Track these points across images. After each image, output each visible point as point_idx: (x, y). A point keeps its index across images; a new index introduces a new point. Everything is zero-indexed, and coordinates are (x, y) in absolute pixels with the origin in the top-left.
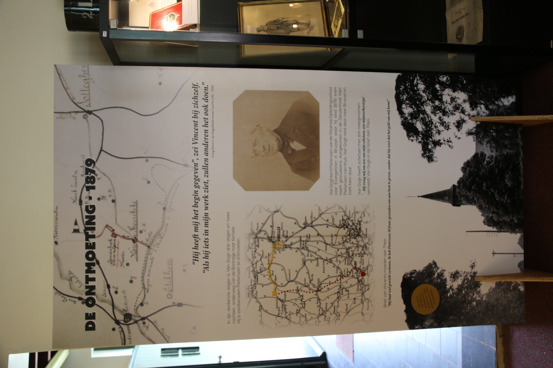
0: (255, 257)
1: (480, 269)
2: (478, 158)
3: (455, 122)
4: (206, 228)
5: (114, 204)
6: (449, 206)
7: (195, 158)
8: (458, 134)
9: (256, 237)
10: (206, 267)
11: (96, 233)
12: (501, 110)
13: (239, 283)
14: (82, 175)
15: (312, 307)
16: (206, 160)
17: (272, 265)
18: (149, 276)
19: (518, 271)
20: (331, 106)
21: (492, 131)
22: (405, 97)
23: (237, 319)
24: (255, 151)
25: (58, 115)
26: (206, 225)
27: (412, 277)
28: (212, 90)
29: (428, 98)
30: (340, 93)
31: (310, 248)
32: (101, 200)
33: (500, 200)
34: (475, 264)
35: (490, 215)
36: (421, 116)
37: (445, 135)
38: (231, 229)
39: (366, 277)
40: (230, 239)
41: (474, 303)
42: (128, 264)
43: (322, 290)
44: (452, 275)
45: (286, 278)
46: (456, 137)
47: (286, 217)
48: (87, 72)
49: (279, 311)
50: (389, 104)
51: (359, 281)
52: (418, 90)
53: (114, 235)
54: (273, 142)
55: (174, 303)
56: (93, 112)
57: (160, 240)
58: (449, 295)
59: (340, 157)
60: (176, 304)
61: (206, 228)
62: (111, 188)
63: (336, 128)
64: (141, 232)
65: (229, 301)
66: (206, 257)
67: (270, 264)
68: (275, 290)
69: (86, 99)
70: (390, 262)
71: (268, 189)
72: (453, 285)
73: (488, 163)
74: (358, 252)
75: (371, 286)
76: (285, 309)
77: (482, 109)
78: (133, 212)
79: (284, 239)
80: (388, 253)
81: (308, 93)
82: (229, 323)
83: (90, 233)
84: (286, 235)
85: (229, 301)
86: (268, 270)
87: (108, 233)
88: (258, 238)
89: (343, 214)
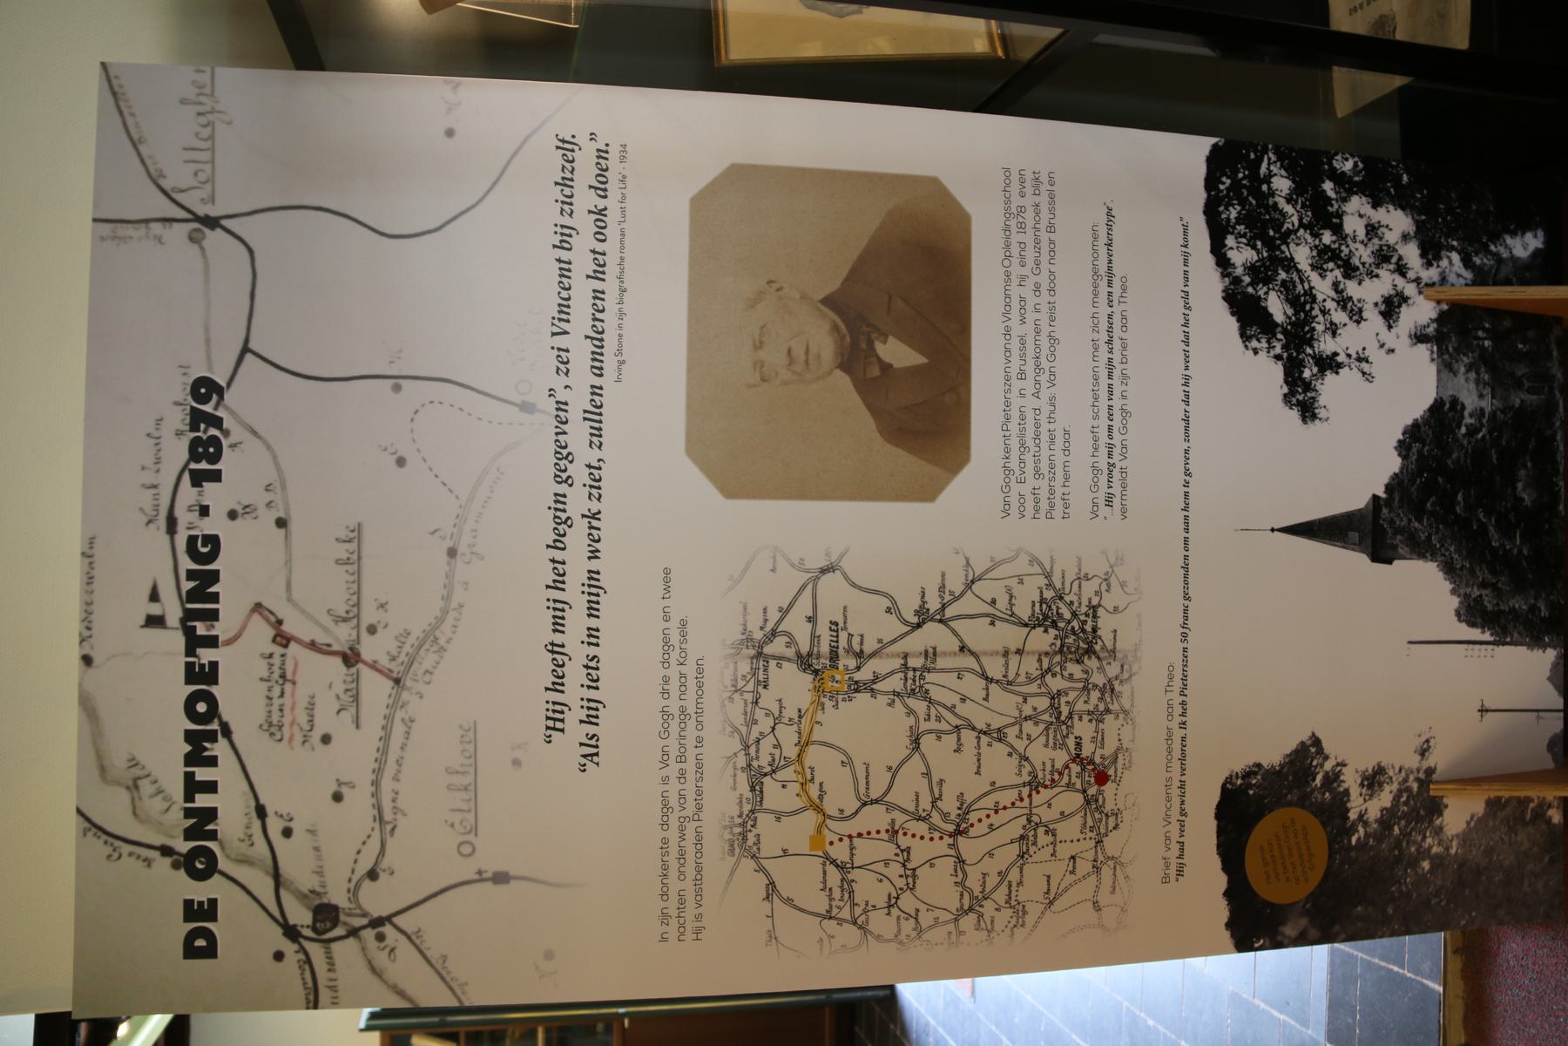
0: (755, 722)
1: (1439, 759)
2: (1442, 414)
3: (1380, 300)
4: (593, 623)
5: (282, 531)
6: (1360, 560)
7: (559, 382)
8: (1387, 337)
9: (760, 654)
10: (591, 752)
11: (220, 629)
12: (1506, 271)
13: (699, 809)
14: (179, 433)
15: (938, 886)
16: (596, 390)
17: (811, 749)
18: (396, 779)
19: (1549, 763)
20: (1007, 229)
21: (1480, 333)
22: (1233, 214)
23: (690, 925)
24: (759, 365)
25: (106, 229)
26: (593, 611)
27: (1250, 786)
28: (623, 159)
29: (1300, 220)
30: (1036, 187)
31: (935, 693)
32: (239, 521)
33: (1502, 545)
34: (1432, 743)
35: (1476, 592)
36: (1283, 275)
37: (1350, 339)
38: (674, 623)
39: (1109, 788)
40: (673, 661)
41: (1426, 865)
42: (326, 739)
43: (972, 832)
44: (1364, 778)
45: (856, 790)
46: (1382, 346)
47: (860, 588)
48: (207, 90)
49: (831, 899)
50: (1185, 232)
51: (1088, 802)
52: (1272, 193)
53: (283, 639)
54: (821, 338)
55: (480, 873)
56: (224, 222)
57: (435, 657)
58: (1354, 840)
59: (1036, 395)
60: (489, 875)
61: (593, 623)
62: (272, 476)
63: (1022, 299)
64: (372, 630)
65: (665, 866)
66: (591, 720)
67: (804, 745)
68: (819, 831)
69: (202, 177)
70: (1183, 739)
71: (802, 495)
72: (1368, 807)
73: (1472, 431)
74: (1086, 707)
75: (1126, 815)
76: (851, 892)
77: (1453, 262)
78: (347, 562)
79: (852, 663)
80: (1178, 710)
81: (934, 182)
82: (664, 939)
83: (201, 629)
84: (857, 648)
85: (665, 866)
86: (796, 766)
87: (261, 632)
88: (767, 658)
89: (1042, 581)
